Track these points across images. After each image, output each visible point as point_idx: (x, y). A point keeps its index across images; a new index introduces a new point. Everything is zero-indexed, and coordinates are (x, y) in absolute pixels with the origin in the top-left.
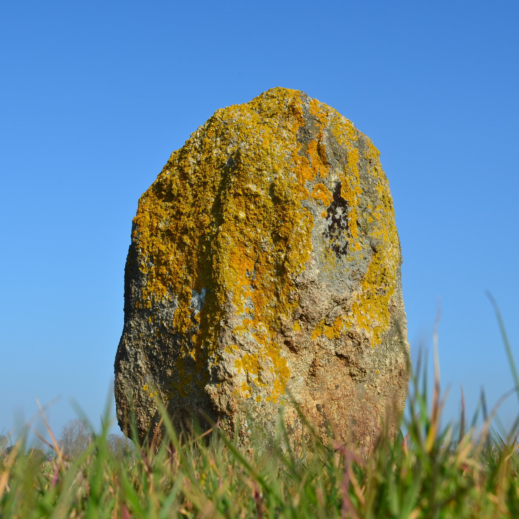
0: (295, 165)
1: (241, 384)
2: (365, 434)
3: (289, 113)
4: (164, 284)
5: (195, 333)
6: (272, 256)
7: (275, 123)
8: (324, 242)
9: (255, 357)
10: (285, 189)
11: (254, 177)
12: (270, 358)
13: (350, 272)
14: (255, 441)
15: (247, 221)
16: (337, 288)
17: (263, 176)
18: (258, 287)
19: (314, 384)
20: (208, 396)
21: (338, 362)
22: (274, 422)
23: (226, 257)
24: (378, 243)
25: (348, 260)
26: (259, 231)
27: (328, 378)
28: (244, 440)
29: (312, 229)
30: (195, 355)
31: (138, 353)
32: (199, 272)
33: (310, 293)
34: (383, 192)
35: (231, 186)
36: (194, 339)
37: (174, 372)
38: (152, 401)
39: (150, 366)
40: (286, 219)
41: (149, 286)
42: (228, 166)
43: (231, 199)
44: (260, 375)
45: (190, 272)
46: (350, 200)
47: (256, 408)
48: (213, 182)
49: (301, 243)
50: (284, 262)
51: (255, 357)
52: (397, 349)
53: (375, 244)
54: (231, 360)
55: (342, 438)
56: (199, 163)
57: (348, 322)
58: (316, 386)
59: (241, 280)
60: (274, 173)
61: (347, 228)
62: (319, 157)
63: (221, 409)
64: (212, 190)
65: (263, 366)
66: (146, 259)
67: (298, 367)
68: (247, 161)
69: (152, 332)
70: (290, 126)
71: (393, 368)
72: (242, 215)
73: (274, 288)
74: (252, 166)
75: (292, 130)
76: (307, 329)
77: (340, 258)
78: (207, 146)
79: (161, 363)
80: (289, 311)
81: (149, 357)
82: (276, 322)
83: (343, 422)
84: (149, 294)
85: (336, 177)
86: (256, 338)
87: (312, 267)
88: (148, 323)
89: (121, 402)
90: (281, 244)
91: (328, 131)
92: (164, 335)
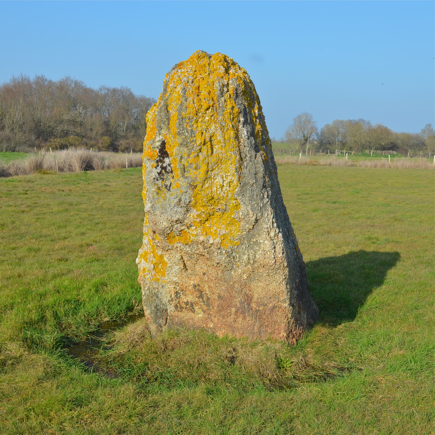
52: (257, 248)
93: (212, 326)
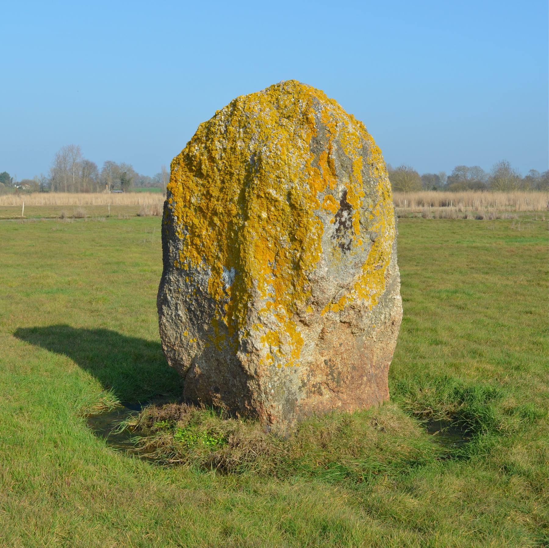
0: (309, 176)
1: (266, 355)
2: (362, 376)
3: (303, 121)
4: (199, 253)
5: (226, 303)
6: (290, 253)
7: (292, 128)
8: (332, 243)
9: (276, 333)
10: (301, 199)
11: (274, 183)
12: (288, 334)
13: (353, 264)
14: (277, 398)
15: (268, 220)
16: (342, 277)
17: (281, 183)
18: (278, 276)
19: (322, 345)
20: (239, 362)
21: (342, 326)
22: (292, 380)
23: (251, 250)
24: (376, 236)
25: (352, 255)
26: (279, 229)
27: (334, 339)
28: (268, 397)
29: (323, 236)
30: (227, 322)
31: (178, 305)
32: (228, 253)
33: (320, 286)
34: (383, 189)
35: (254, 188)
36: (226, 308)
37: (210, 328)
38: (192, 346)
39: (189, 317)
40: (301, 225)
41: (185, 251)
42: (251, 164)
43: (254, 198)
44: (280, 348)
45: (221, 250)
46: (354, 204)
47: (277, 373)
48: (238, 175)
49: (313, 247)
50: (299, 261)
51: (276, 333)
52: (391, 305)
53: (374, 237)
54: (258, 336)
55: (344, 382)
56: (225, 150)
57: (351, 297)
58: (325, 346)
59: (264, 269)
60: (290, 182)
61: (351, 227)
62: (329, 168)
63: (250, 373)
64: (237, 182)
65: (283, 341)
66: (182, 226)
67: (310, 336)
68: (268, 168)
69: (190, 291)
70: (304, 136)
71: (387, 321)
72: (264, 215)
73: (291, 279)
74: (272, 174)
75: (305, 140)
76: (318, 310)
77: (345, 253)
78: (232, 135)
79: (198, 318)
80: (303, 299)
81: (188, 309)
82: (292, 306)
83: (345, 369)
84: (186, 258)
85: (343, 187)
86: (277, 318)
87: (322, 266)
88: (186, 282)
89: (165, 341)
90: (297, 243)
91: (337, 142)
92: (199, 296)
93: (340, 404)
